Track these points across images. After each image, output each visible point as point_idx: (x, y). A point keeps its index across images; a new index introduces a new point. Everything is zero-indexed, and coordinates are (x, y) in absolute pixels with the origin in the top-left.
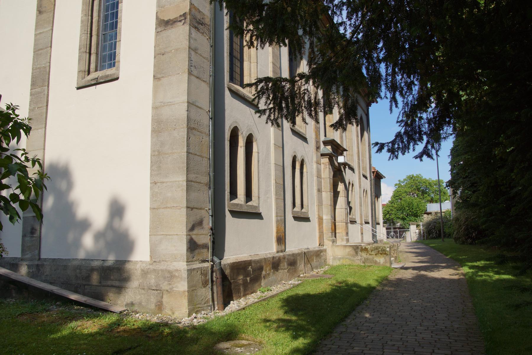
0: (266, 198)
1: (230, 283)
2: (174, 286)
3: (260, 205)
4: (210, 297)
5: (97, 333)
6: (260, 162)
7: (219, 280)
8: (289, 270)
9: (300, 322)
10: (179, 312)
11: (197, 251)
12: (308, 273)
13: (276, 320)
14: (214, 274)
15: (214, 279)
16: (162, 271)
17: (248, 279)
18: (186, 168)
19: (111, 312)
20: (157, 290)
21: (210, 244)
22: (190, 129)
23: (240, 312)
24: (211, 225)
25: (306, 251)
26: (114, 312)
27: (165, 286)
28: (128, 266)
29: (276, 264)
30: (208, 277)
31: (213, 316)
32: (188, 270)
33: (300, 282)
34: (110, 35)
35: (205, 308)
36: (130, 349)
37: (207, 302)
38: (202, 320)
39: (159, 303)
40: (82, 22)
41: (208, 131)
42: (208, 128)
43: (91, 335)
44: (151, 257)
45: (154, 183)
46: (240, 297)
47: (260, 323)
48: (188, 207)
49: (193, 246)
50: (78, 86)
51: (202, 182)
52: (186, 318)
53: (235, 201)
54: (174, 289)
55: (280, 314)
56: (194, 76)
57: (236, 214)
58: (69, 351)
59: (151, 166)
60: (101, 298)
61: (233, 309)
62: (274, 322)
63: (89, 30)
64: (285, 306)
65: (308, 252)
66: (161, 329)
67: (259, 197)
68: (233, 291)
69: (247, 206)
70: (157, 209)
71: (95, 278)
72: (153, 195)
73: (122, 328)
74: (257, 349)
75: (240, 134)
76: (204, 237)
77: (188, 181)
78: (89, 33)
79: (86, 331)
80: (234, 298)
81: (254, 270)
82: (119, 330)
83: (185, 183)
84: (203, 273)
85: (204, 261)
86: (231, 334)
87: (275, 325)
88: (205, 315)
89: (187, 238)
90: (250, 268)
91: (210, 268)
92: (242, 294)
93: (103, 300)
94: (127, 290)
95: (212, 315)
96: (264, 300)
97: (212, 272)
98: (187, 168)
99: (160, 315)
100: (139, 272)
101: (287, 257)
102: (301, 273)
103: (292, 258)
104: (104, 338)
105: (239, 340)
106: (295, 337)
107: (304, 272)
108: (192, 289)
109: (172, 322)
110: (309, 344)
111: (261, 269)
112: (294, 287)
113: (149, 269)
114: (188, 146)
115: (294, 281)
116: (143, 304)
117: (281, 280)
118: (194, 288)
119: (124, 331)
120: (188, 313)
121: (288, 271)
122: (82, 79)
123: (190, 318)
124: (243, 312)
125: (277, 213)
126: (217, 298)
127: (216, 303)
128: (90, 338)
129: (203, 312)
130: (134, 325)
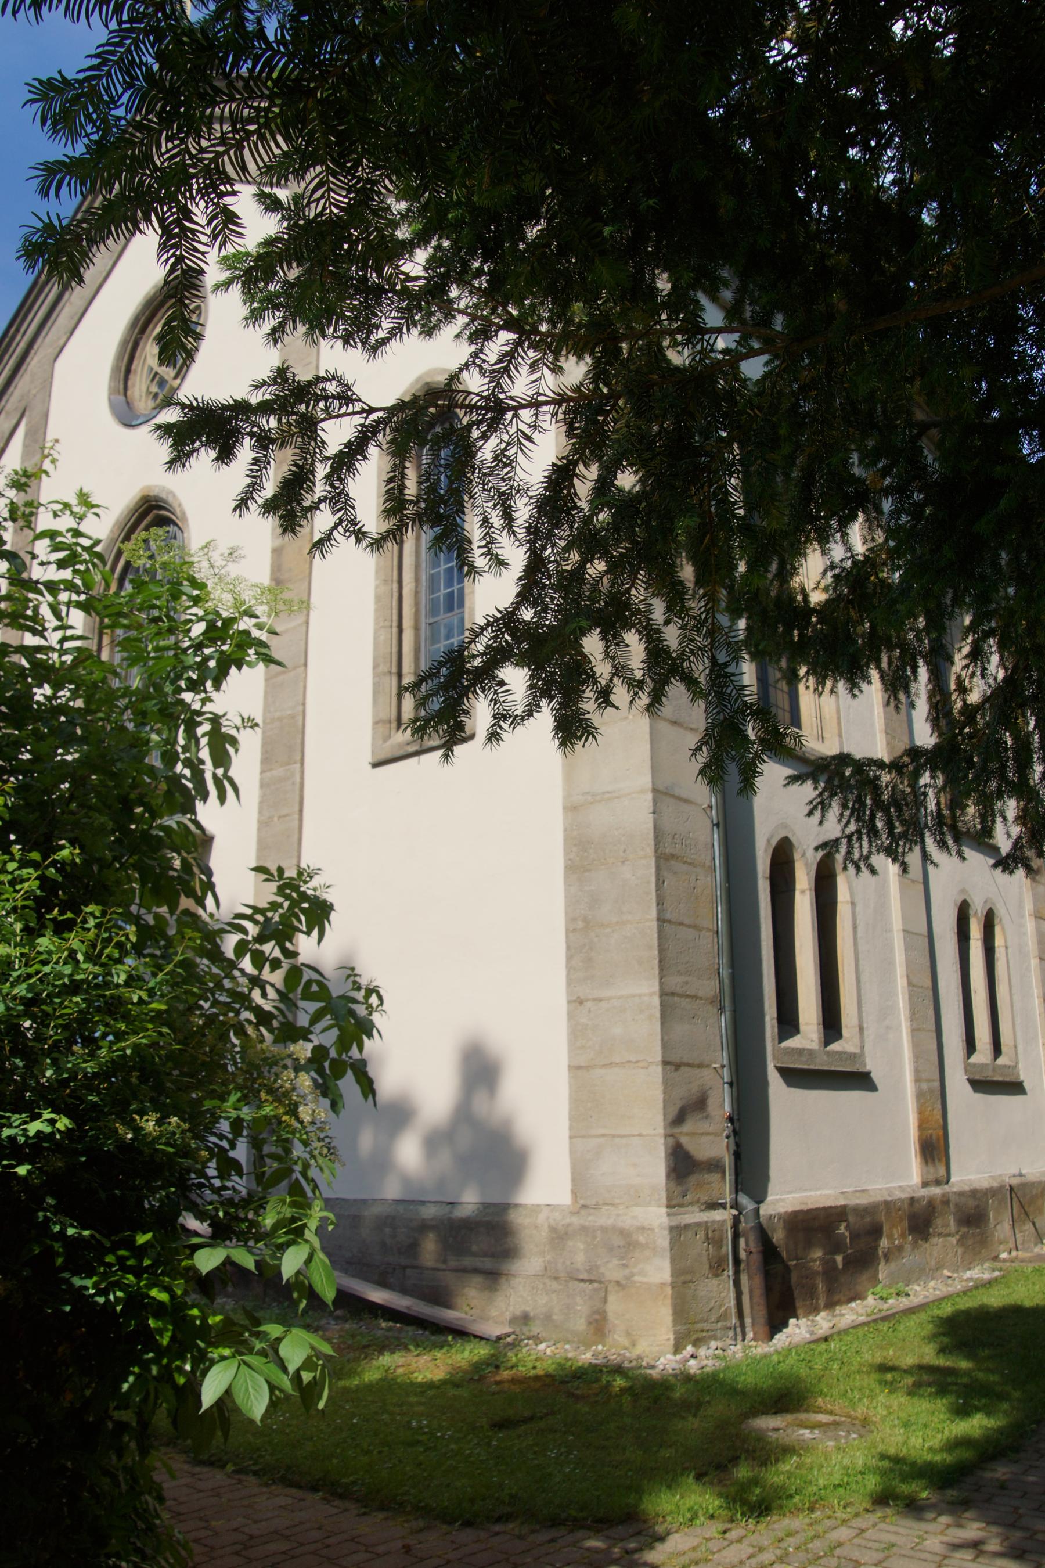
0: (883, 1027)
1: (787, 1267)
2: (635, 1270)
3: (867, 1049)
4: (732, 1303)
5: (444, 1382)
6: (860, 929)
7: (756, 1258)
8: (963, 1237)
9: (981, 1375)
10: (649, 1340)
11: (693, 1179)
12: (1025, 1250)
13: (912, 1367)
14: (742, 1242)
15: (743, 1255)
16: (604, 1229)
17: (839, 1259)
18: (656, 962)
19: (475, 1336)
20: (591, 1281)
21: (728, 1161)
22: (663, 859)
23: (813, 1346)
24: (727, 1108)
25: (1015, 1181)
26: (481, 1338)
27: (611, 1270)
28: (518, 1218)
29: (920, 1220)
30: (724, 1250)
31: (743, 1353)
32: (672, 1229)
33: (997, 1274)
34: (445, 626)
35: (719, 1334)
36: (531, 1419)
37: (724, 1317)
38: (710, 1363)
39: (597, 1317)
40: (378, 599)
41: (709, 858)
42: (709, 852)
43: (430, 1385)
44: (574, 1193)
45: (576, 1002)
46: (816, 1310)
47: (869, 1373)
48: (665, 1063)
49: (682, 1166)
50: (376, 760)
51: (700, 994)
52: (670, 1356)
53: (792, 1043)
54: (636, 1278)
55: (929, 1355)
56: (666, 720)
57: (799, 1077)
58: (385, 1416)
59: (569, 958)
60: (440, 1297)
61: (796, 1339)
62: (907, 1372)
63: (395, 617)
64: (944, 1334)
65: (1023, 1185)
66: (604, 1379)
67: (861, 1029)
68: (796, 1293)
69: (828, 1053)
70: (587, 1068)
71: (430, 1248)
72: (577, 1034)
73: (506, 1374)
74: (854, 1436)
75: (797, 856)
76: (712, 1142)
77: (664, 994)
78: (395, 624)
79: (419, 1378)
80: (800, 1312)
81: (855, 1236)
82: (498, 1378)
83: (656, 1001)
84: (713, 1237)
85: (713, 1206)
86: (787, 1397)
87: (910, 1380)
88: (719, 1352)
89: (666, 1144)
90: (842, 1229)
91: (729, 1224)
92: (822, 1302)
93: (448, 1306)
94: (514, 1282)
95: (736, 1351)
96: (884, 1319)
97: (736, 1236)
98: (660, 961)
99: (600, 1347)
100: (545, 1233)
101: (953, 1199)
102: (1002, 1247)
103: (971, 1203)
104: (464, 1392)
105: (807, 1411)
106: (962, 1412)
107: (1011, 1245)
108: (682, 1278)
109: (634, 1364)
110: (1000, 1431)
111: (876, 1231)
112: (976, 1287)
113: (569, 1225)
114: (660, 902)
115: (979, 1273)
116: (555, 1317)
117: (939, 1267)
118: (688, 1277)
119: (513, 1381)
120: (672, 1342)
121: (961, 1242)
122: (385, 741)
123: (678, 1357)
124: (823, 1346)
125: (917, 1071)
126: (752, 1307)
127: (748, 1321)
128: (430, 1393)
129: (713, 1344)
130: (534, 1368)
